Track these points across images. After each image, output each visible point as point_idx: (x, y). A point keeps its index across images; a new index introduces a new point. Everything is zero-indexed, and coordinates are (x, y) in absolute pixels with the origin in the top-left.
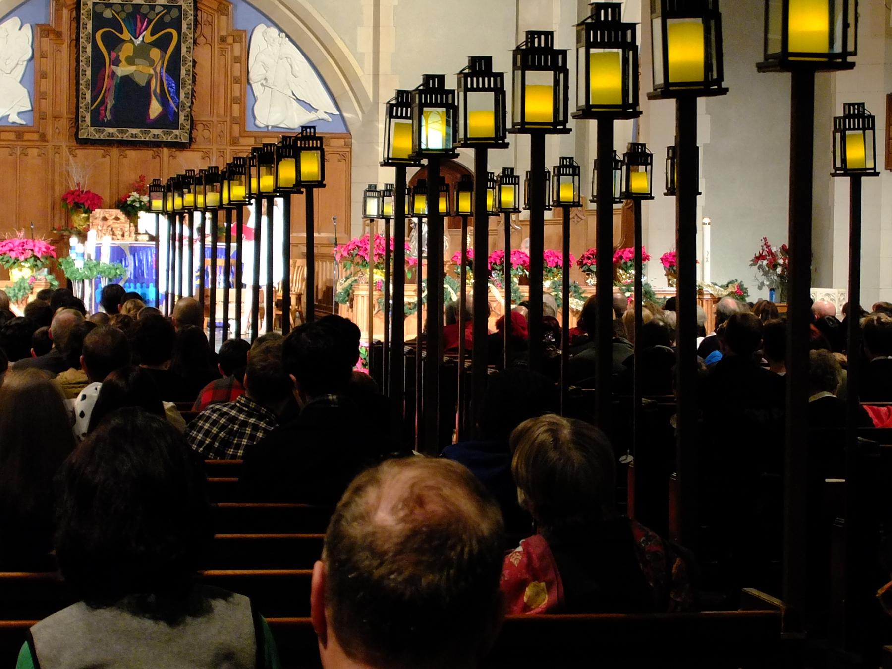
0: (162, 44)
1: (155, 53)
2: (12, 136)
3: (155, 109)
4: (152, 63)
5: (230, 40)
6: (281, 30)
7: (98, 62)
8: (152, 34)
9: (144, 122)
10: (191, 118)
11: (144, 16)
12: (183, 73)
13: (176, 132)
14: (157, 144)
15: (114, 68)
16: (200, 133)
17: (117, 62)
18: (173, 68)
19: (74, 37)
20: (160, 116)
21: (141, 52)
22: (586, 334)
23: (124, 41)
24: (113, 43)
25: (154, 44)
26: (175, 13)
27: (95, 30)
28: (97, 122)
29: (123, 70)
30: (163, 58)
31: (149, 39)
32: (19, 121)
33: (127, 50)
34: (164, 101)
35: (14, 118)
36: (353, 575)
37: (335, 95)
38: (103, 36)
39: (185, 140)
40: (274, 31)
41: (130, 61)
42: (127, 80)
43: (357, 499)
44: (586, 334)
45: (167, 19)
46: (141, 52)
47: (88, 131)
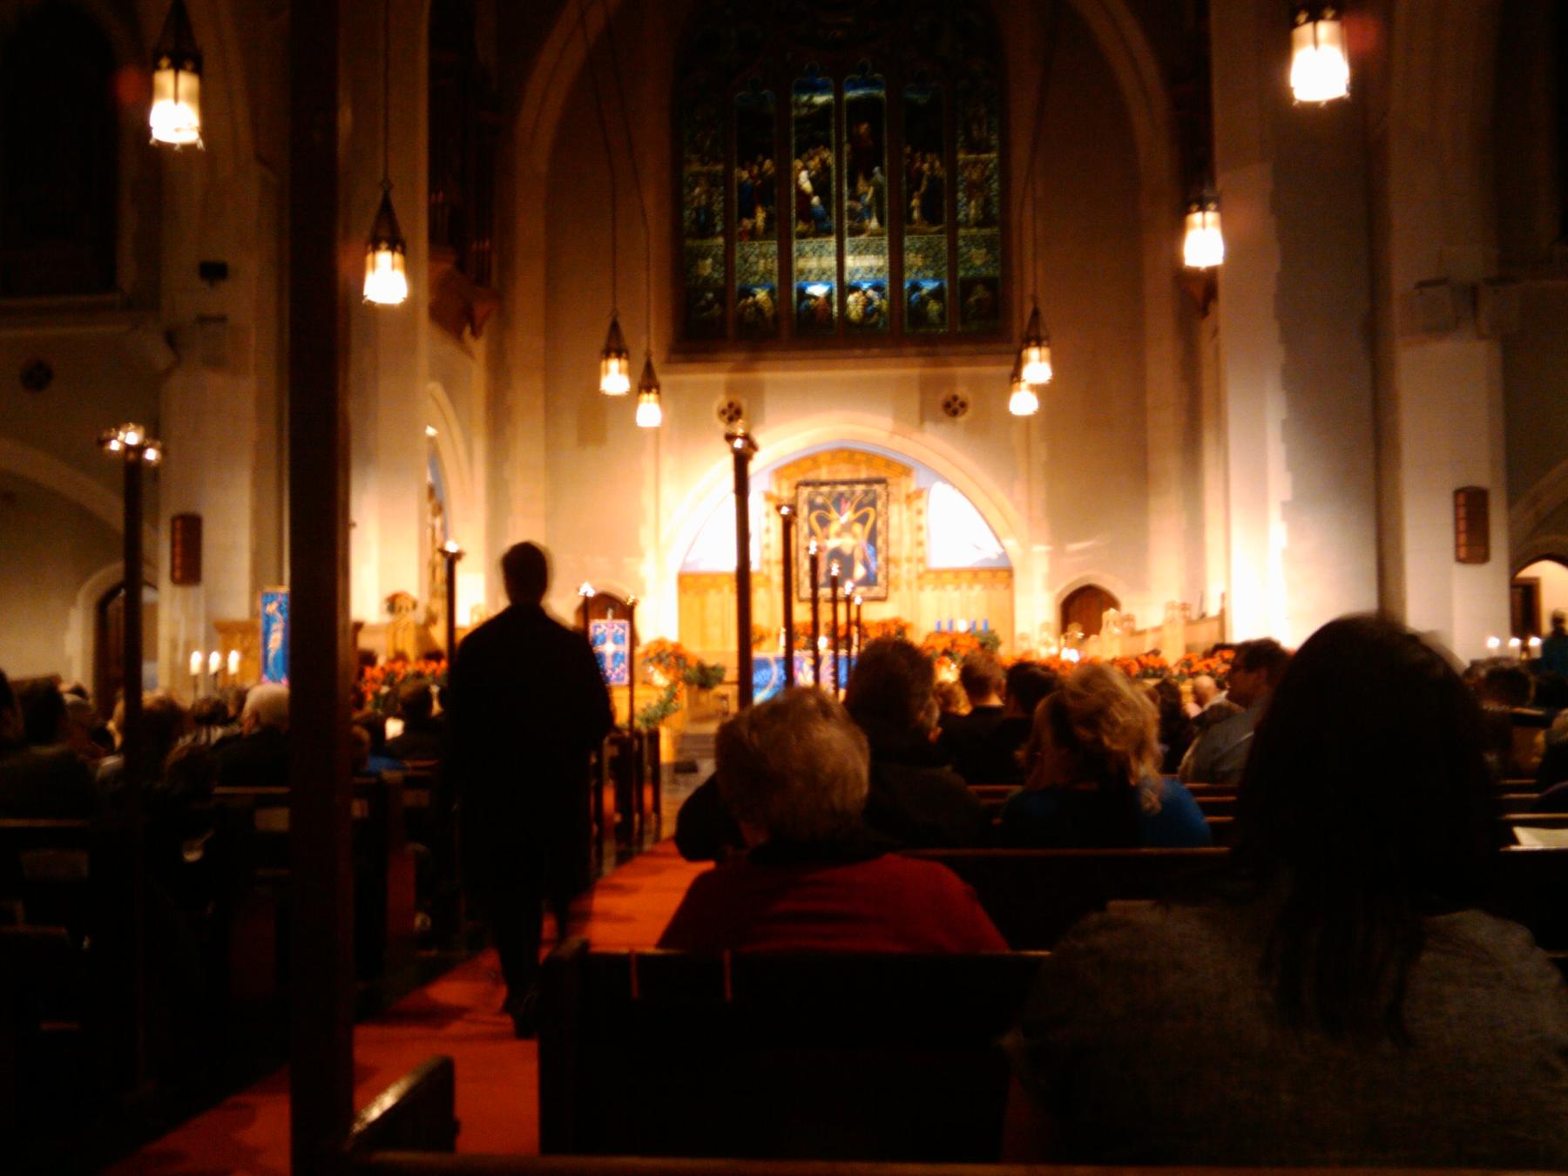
0: (863, 520)
1: (857, 528)
4: (855, 536)
6: (954, 486)
10: (887, 577)
16: (893, 595)
17: (827, 537)
18: (872, 538)
19: (880, 541)
22: (174, 117)
24: (824, 522)
26: (871, 496)
33: (834, 528)
34: (866, 565)
36: (713, 526)
37: (732, 499)
39: (882, 594)
40: (948, 488)
41: (838, 535)
43: (668, 463)
44: (174, 117)
46: (847, 528)
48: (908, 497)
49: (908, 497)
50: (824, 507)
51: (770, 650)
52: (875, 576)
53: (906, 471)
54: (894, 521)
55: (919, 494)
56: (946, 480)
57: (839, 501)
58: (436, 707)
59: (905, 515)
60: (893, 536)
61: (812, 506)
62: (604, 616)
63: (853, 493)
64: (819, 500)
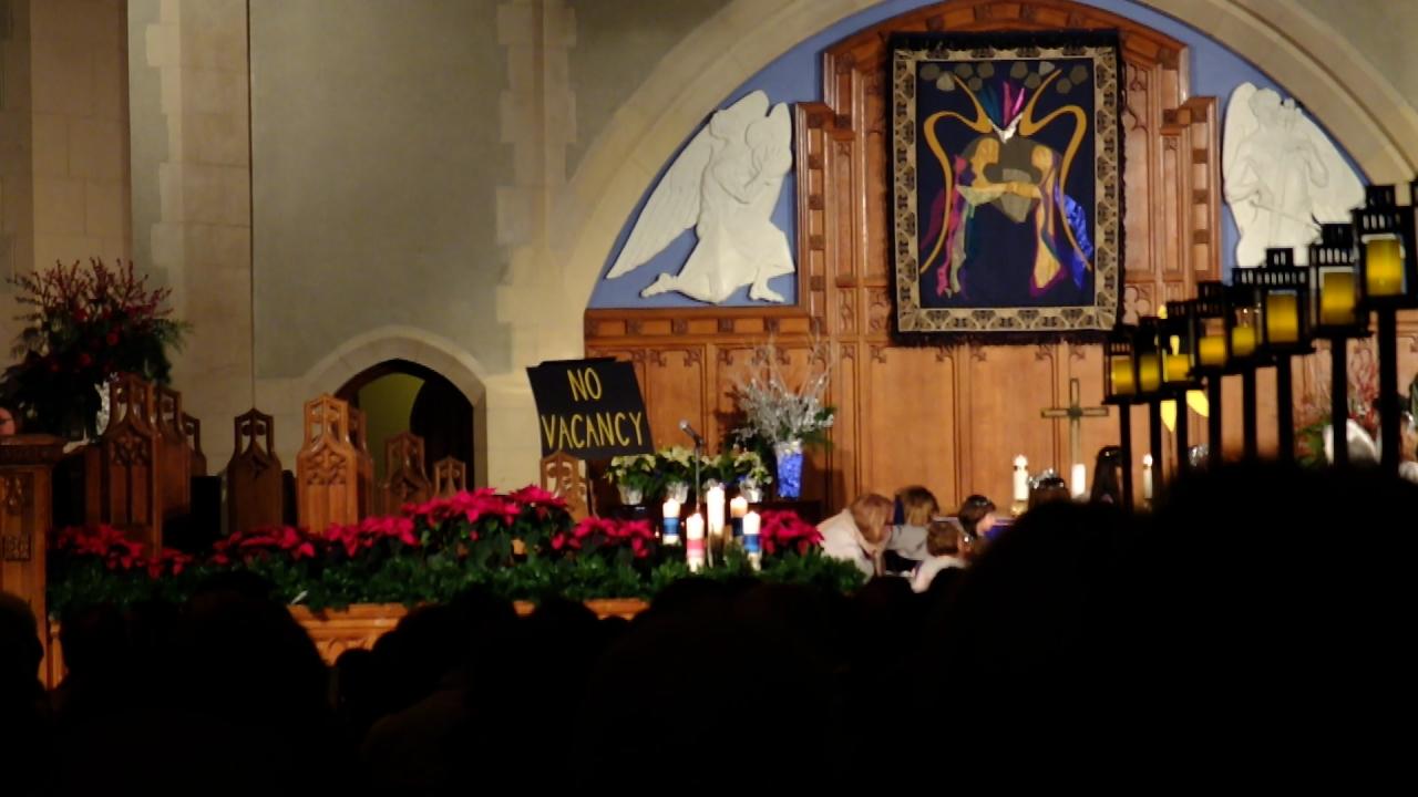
0: (1055, 137)
1: (1043, 158)
2: (758, 325)
3: (1046, 267)
4: (1036, 176)
5: (1185, 117)
7: (930, 181)
8: (1035, 119)
9: (1028, 297)
11: (1017, 84)
12: (1100, 192)
13: (1090, 311)
14: (1046, 338)
15: (960, 189)
17: (967, 178)
18: (1080, 182)
20: (1056, 284)
21: (1015, 157)
23: (978, 135)
24: (960, 140)
25: (1040, 138)
26: (1079, 74)
27: (922, 116)
28: (931, 298)
29: (981, 192)
30: (1057, 164)
31: (1029, 129)
32: (772, 296)
33: (985, 154)
34: (1062, 249)
35: (762, 292)
38: (938, 127)
41: (994, 174)
42: (989, 213)
45: (1064, 87)
47: (915, 317)
48: (1170, 117)
49: (1170, 117)
50: (959, 101)
51: (711, 395)
52: (1089, 278)
53: (1166, 52)
54: (1136, 178)
55: (1197, 109)
56: (1264, 78)
57: (999, 89)
58: (52, 670)
59: (1167, 163)
60: (1136, 218)
61: (928, 98)
62: (684, 486)
63: (1034, 66)
64: (946, 83)
